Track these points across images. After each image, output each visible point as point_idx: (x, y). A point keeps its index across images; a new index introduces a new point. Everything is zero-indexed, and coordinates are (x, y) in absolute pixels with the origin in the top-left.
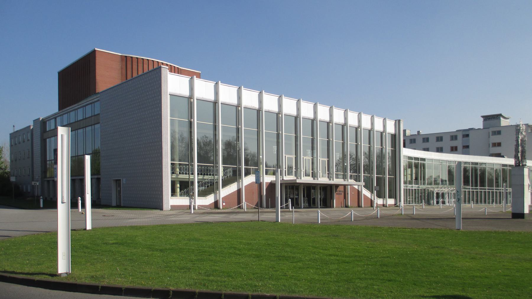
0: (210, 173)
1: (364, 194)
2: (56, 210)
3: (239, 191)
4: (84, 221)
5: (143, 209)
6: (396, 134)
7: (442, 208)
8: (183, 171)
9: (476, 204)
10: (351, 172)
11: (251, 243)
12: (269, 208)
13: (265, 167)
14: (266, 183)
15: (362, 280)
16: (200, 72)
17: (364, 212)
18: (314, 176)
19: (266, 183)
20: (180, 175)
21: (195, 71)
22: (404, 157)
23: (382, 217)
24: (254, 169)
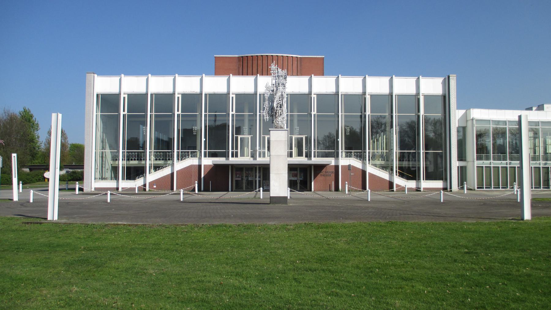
0: (116, 158)
1: (369, 173)
2: (10, 191)
3: (172, 174)
4: (439, 195)
5: (71, 190)
6: (445, 94)
7: (407, 194)
8: (144, 158)
9: (535, 188)
10: (320, 148)
11: (137, 225)
12: (228, 191)
13: (232, 150)
14: (204, 165)
15: (402, 277)
16: (324, 57)
17: (384, 195)
18: (308, 156)
19: (204, 165)
20: (169, 161)
21: (318, 57)
22: (528, 123)
23: (446, 203)
24: (320, 149)
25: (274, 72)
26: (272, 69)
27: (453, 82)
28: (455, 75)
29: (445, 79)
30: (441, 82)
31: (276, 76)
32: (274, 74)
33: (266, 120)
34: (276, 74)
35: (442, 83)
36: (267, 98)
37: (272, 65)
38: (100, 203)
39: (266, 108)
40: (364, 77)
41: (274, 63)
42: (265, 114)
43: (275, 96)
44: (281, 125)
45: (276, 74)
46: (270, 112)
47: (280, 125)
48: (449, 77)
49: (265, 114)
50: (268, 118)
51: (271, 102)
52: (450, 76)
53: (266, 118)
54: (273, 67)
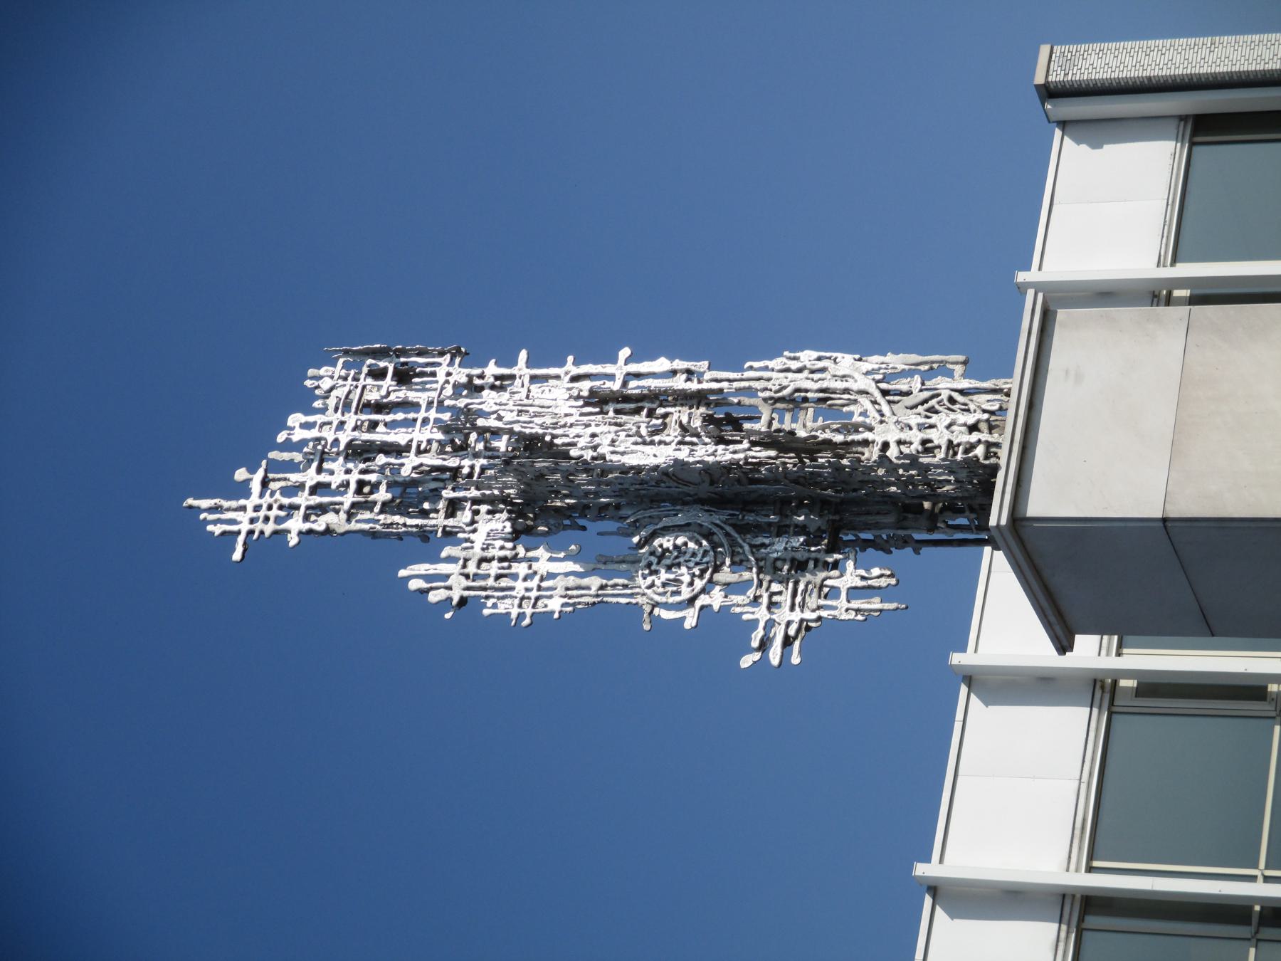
6: (1183, 118)
25: (303, 499)
26: (269, 528)
27: (1093, 58)
28: (1045, 49)
29: (1064, 124)
30: (1084, 147)
31: (354, 478)
32: (322, 509)
33: (876, 604)
34: (337, 471)
35: (1096, 145)
36: (595, 582)
37: (217, 529)
38: (428, 528)
39: (716, 599)
40: (964, 689)
41: (205, 503)
42: (796, 616)
43: (640, 587)
44: (971, 419)
45: (335, 481)
46: (779, 547)
47: (973, 428)
48: (1051, 92)
49: (796, 616)
50: (851, 576)
51: (647, 541)
52: (1039, 79)
53: (854, 592)
54: (243, 518)
